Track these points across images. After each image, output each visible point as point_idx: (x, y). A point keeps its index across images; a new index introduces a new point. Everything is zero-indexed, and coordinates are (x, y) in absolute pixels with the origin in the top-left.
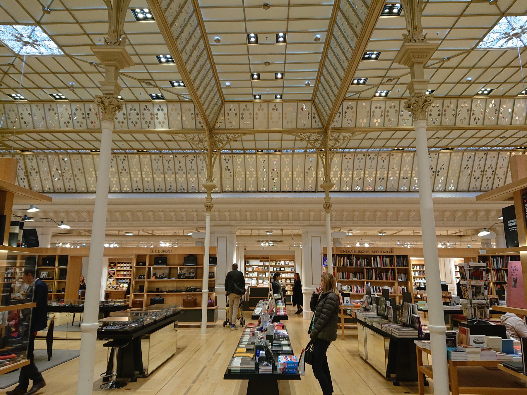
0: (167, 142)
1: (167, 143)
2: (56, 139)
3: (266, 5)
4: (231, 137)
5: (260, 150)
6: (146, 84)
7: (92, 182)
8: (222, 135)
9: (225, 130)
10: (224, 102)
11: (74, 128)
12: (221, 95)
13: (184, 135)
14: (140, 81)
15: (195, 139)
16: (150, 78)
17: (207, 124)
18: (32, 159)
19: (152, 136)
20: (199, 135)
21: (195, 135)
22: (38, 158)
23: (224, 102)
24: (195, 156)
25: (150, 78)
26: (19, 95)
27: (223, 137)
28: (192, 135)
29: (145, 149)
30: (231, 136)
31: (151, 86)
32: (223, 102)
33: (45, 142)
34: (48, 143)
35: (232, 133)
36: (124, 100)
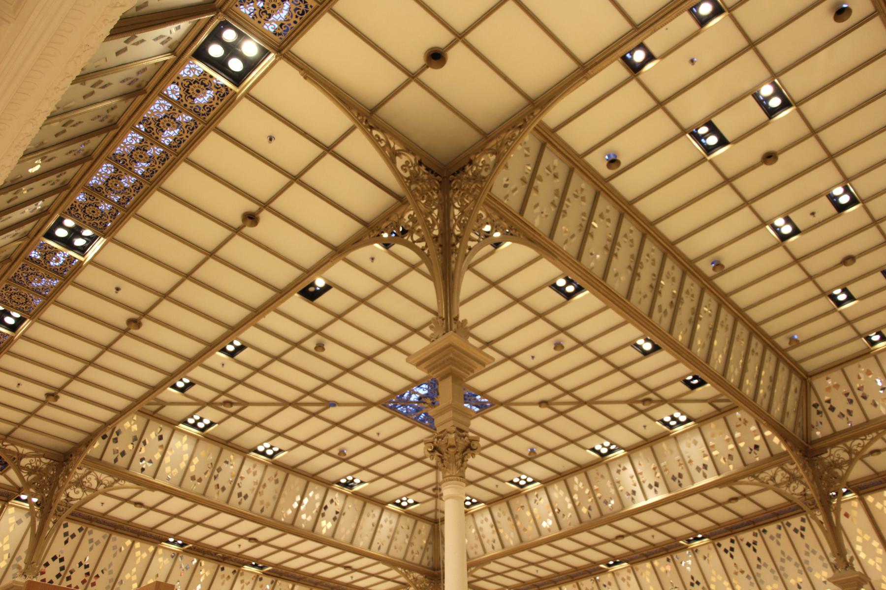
0: (730, 505)
1: (731, 505)
2: (491, 574)
3: (320, 346)
4: (855, 448)
5: (691, 538)
6: (644, 404)
7: (879, 568)
8: (833, 450)
9: (837, 437)
10: (807, 379)
11: (719, 474)
12: (794, 367)
13: (753, 476)
14: (631, 402)
15: (778, 479)
16: (642, 390)
17: (785, 436)
18: (779, 536)
19: (697, 501)
20: (784, 467)
21: (774, 470)
22: (790, 529)
23: (807, 379)
24: (670, 558)
25: (642, 390)
26: (523, 477)
27: (838, 453)
28: (770, 472)
29: (697, 532)
30: (856, 444)
31: (653, 404)
32: (805, 380)
33: (740, 501)
34: (630, 538)
35: (855, 438)
36: (694, 420)
